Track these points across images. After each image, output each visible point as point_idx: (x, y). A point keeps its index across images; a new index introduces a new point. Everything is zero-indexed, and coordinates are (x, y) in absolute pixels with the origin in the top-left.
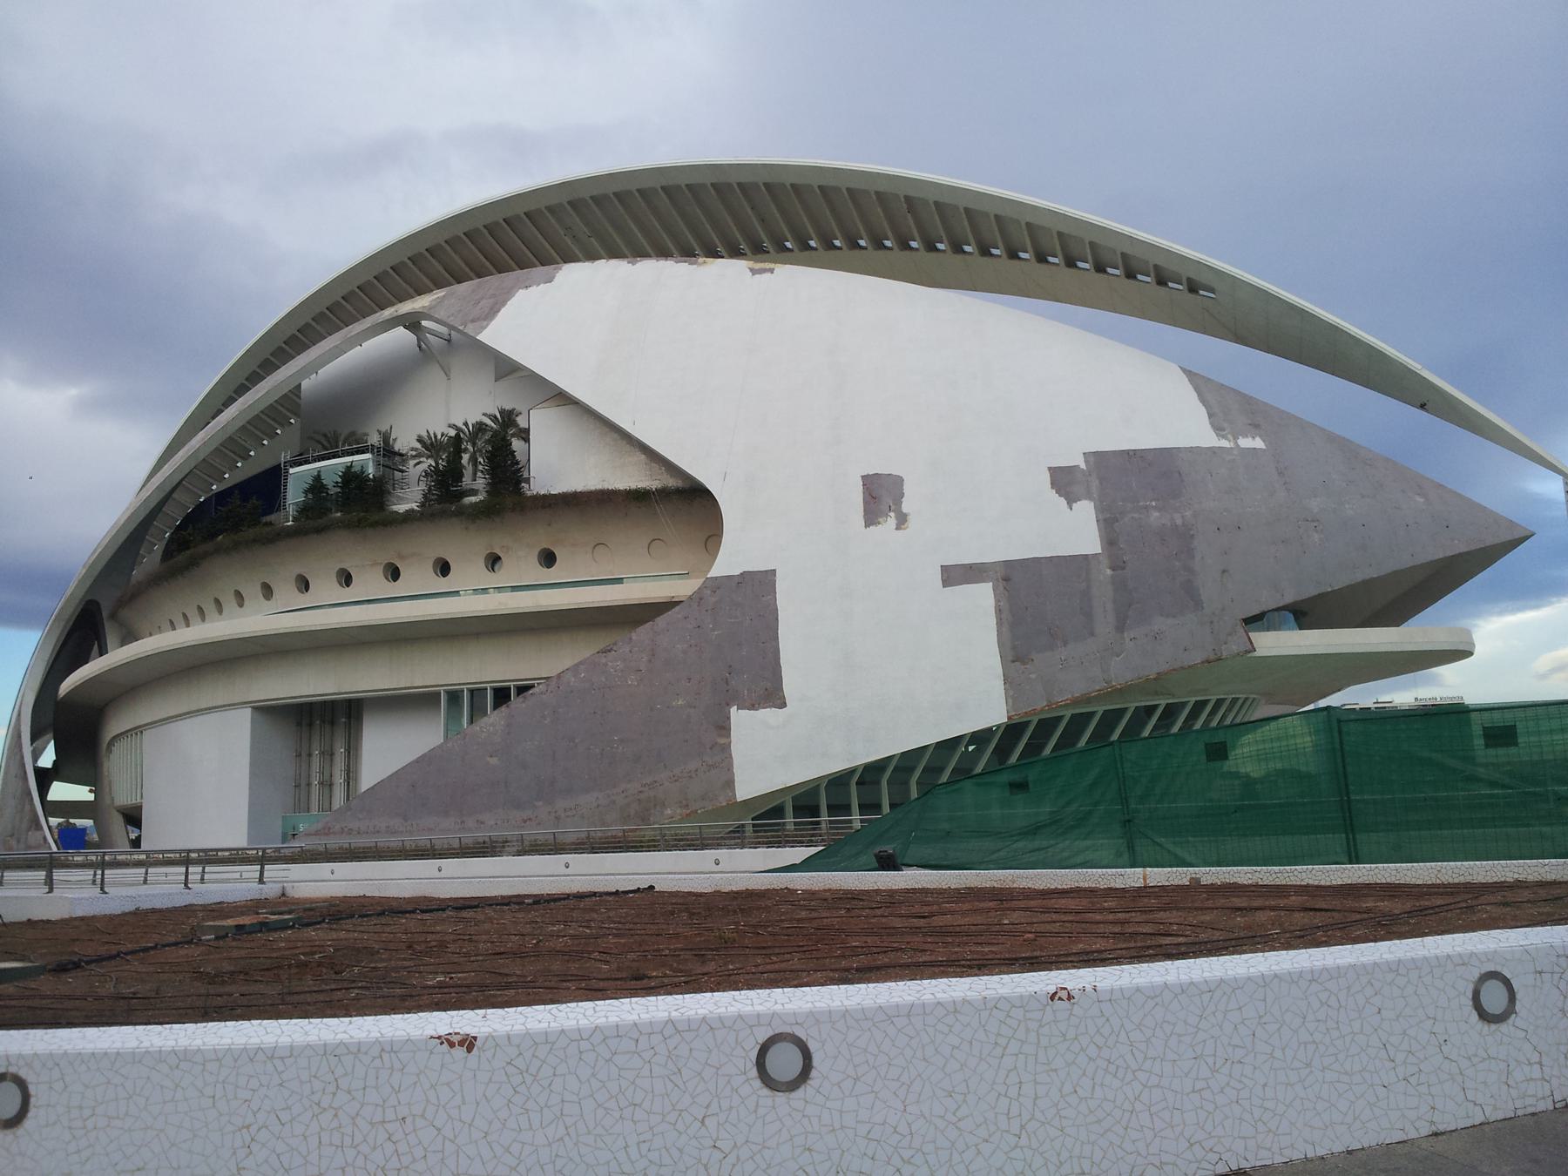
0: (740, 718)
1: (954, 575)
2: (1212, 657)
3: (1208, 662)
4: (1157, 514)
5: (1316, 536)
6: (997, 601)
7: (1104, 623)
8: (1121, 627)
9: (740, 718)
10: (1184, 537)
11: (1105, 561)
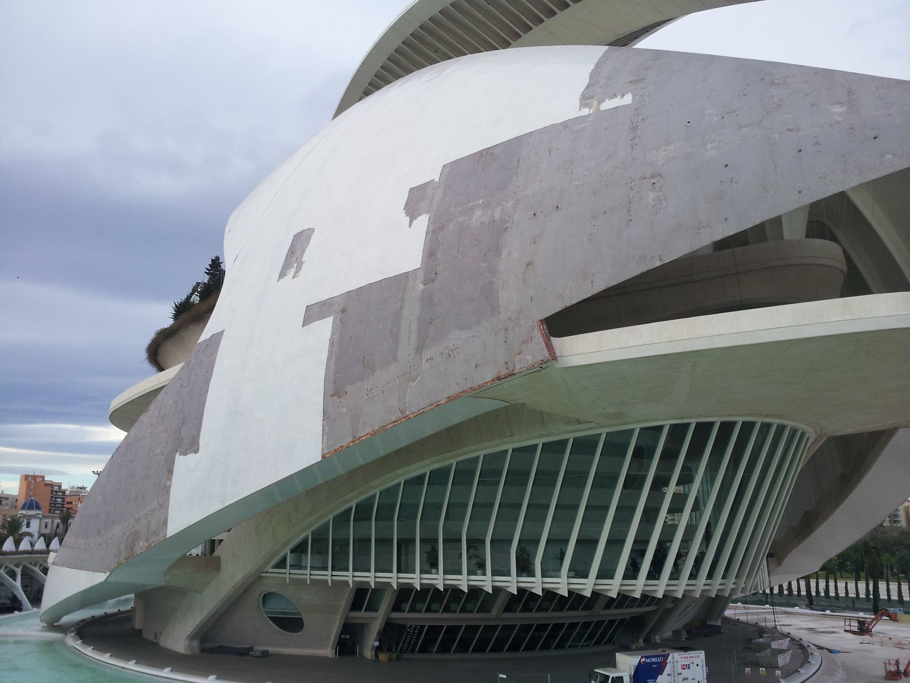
0: (179, 460)
1: (313, 314)
2: (504, 372)
3: (499, 379)
4: (479, 213)
5: (652, 196)
6: (333, 334)
7: (406, 349)
8: (419, 349)
9: (179, 460)
10: (498, 230)
11: (421, 276)
